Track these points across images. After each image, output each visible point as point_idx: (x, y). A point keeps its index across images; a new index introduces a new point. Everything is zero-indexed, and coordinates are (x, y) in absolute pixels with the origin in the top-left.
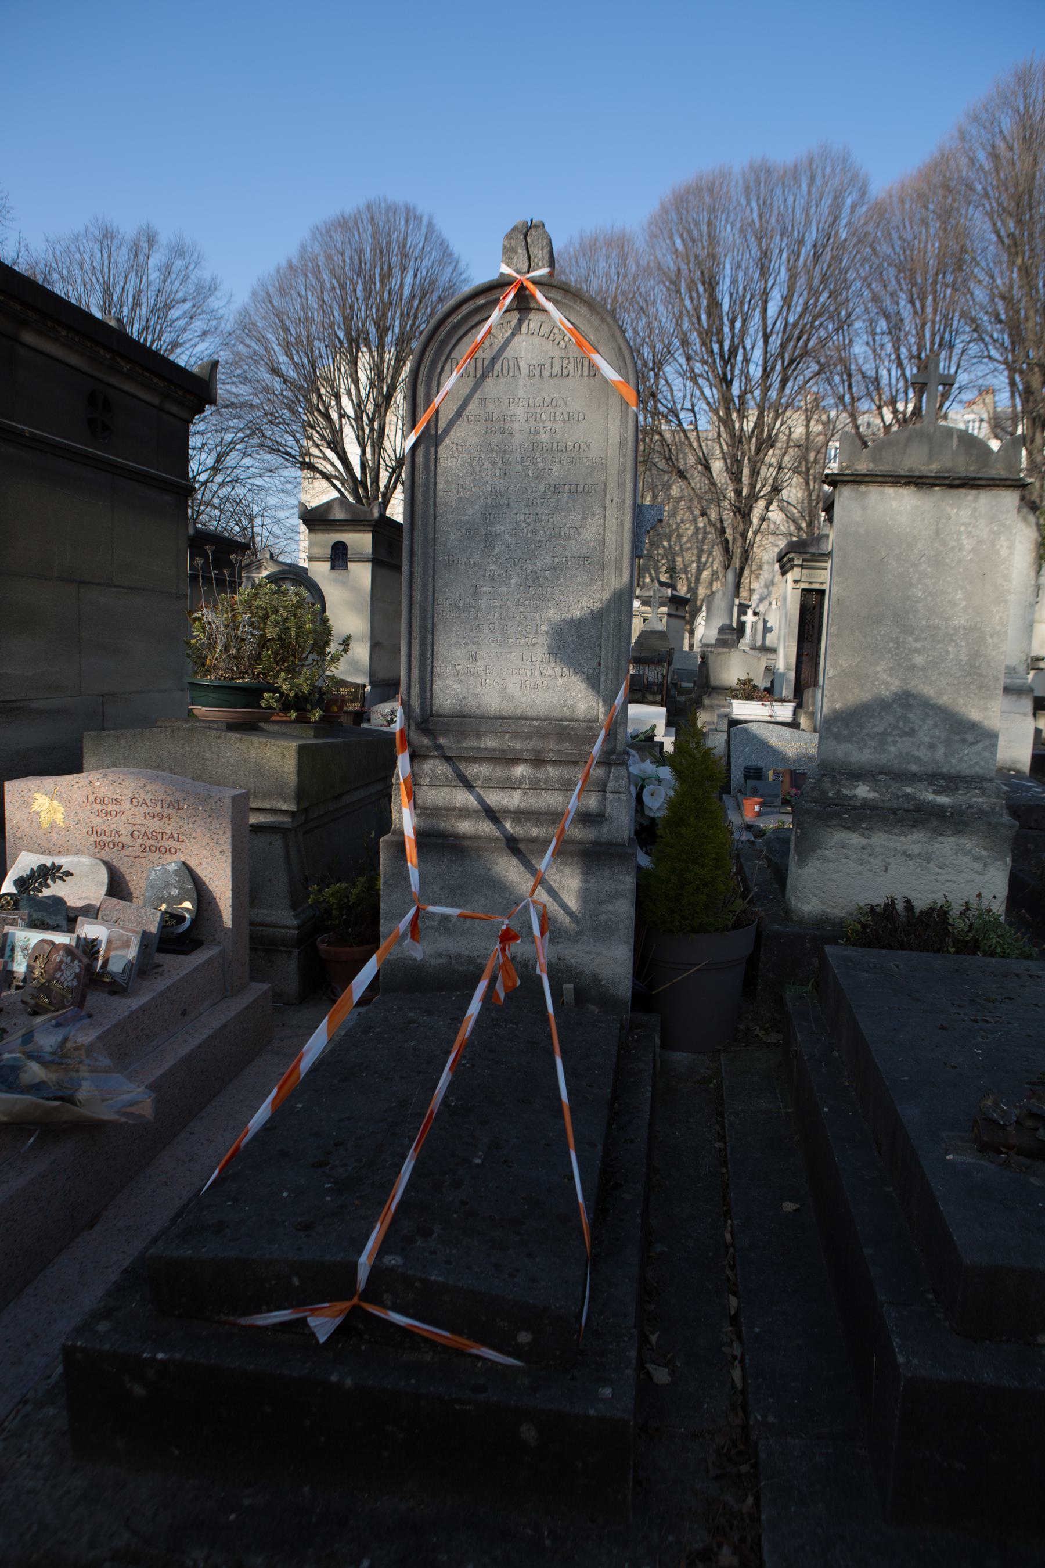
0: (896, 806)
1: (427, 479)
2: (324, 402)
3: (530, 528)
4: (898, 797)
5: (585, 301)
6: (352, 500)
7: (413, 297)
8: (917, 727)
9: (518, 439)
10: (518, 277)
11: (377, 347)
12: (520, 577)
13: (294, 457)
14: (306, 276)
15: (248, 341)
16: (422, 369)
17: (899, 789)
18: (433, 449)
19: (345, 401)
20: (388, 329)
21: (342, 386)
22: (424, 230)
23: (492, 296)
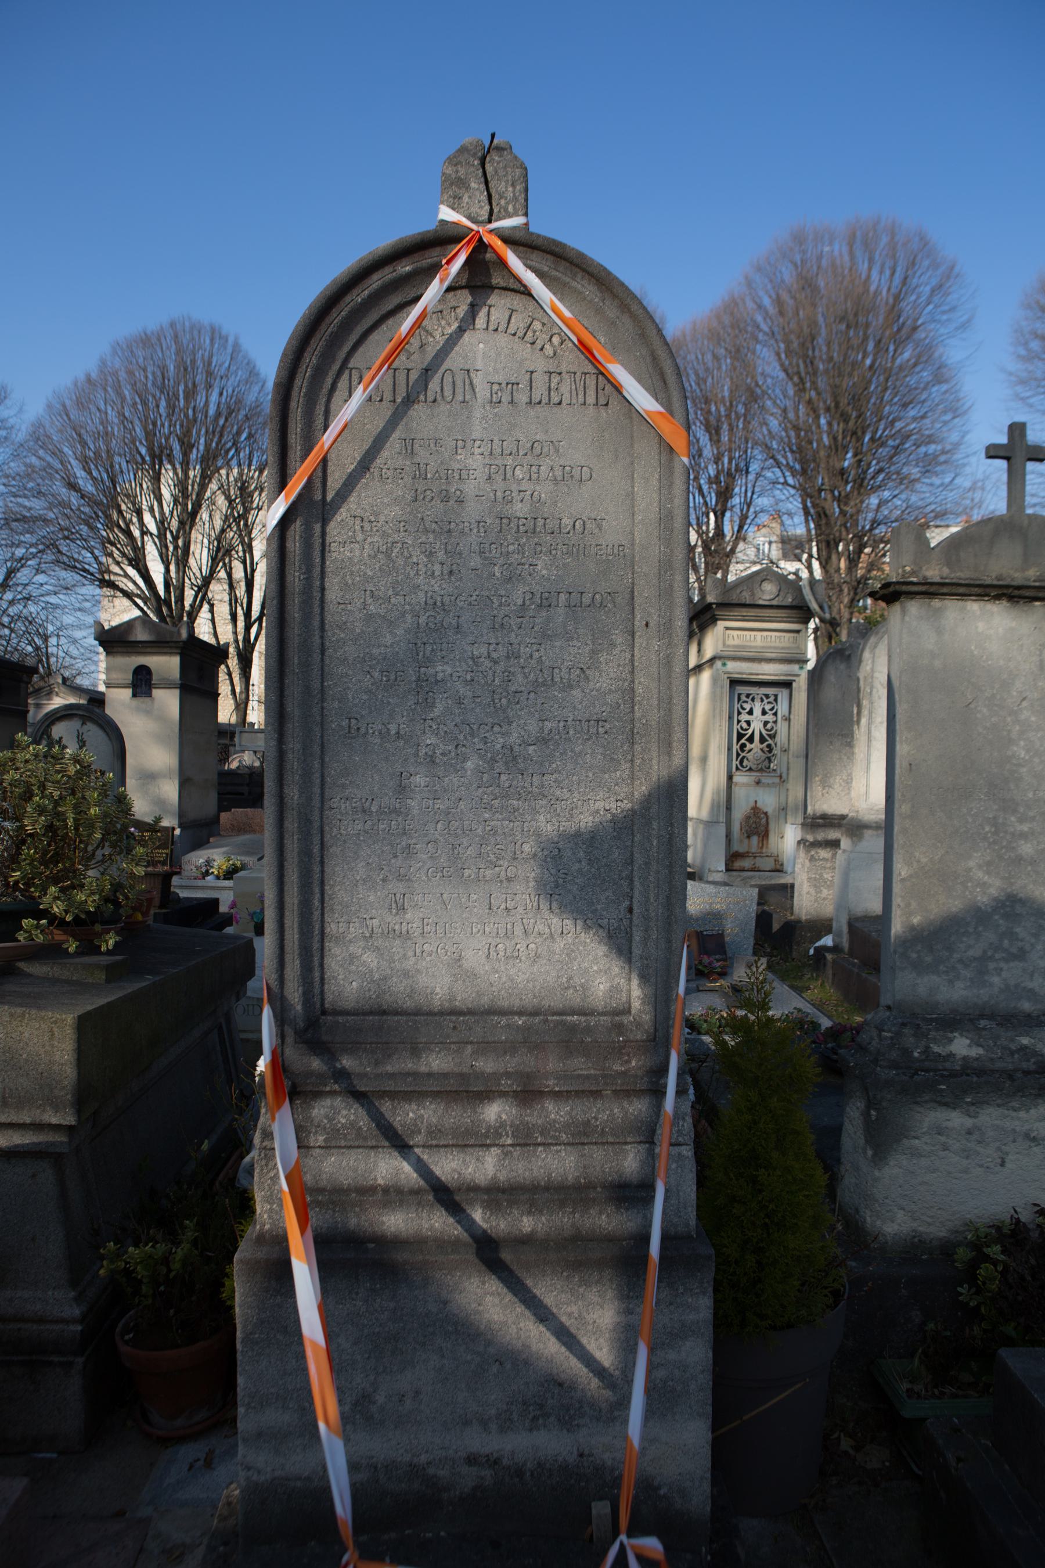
0: (1011, 1067)
1: (309, 579)
2: (124, 518)
3: (499, 669)
4: (1012, 1053)
5: (588, 273)
6: (155, 619)
7: (218, 415)
8: (1028, 947)
9: (472, 511)
10: (474, 227)
11: (181, 464)
12: (481, 757)
13: (92, 574)
14: (105, 390)
15: (41, 452)
16: (298, 382)
17: (1012, 1040)
18: (318, 527)
19: (147, 518)
20: (193, 446)
21: (144, 502)
22: (229, 350)
23: (425, 260)
